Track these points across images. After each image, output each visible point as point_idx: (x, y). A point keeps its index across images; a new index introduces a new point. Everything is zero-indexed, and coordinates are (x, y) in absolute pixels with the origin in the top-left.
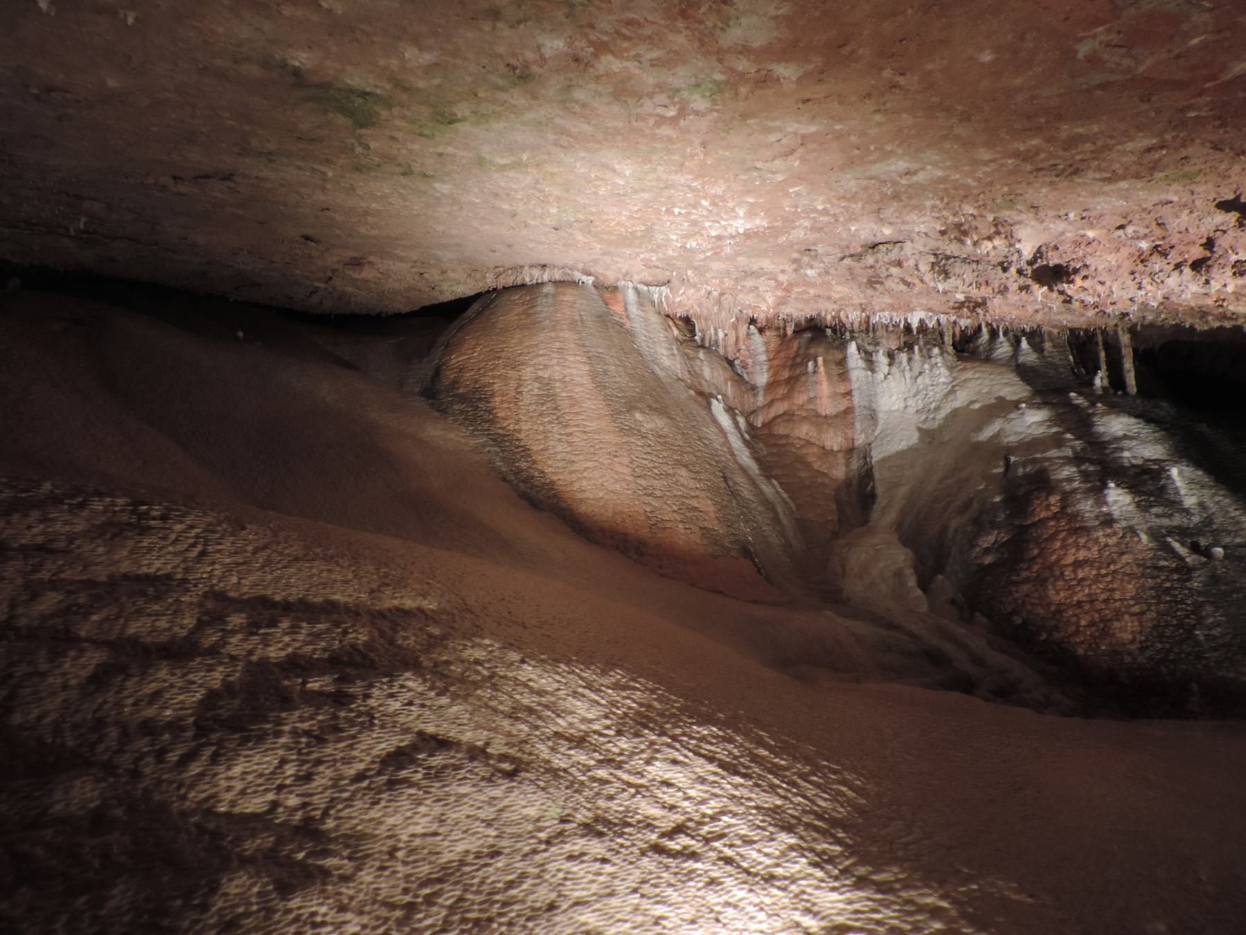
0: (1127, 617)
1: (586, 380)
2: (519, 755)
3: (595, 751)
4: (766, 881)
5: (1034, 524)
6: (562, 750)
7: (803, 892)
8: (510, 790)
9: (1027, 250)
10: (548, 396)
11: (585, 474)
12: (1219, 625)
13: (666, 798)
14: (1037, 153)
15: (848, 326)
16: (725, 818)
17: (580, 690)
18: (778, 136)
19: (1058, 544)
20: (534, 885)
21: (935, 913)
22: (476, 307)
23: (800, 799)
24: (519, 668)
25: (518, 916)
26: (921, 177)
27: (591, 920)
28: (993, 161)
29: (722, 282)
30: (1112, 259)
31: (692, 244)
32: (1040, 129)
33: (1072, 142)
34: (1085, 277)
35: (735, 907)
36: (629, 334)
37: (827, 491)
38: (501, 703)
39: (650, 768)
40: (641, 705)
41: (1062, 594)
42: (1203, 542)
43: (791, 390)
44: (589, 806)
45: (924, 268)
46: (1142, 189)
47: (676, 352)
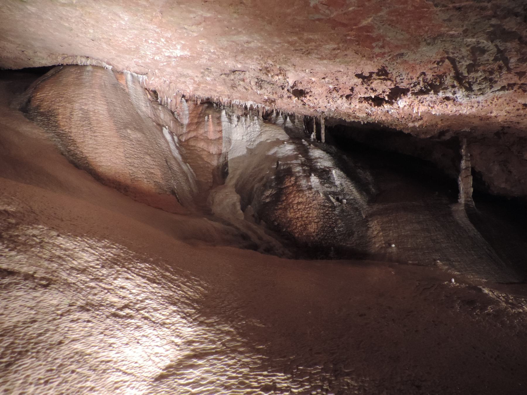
0: (313, 223)
1: (105, 113)
2: (51, 277)
3: (90, 275)
4: (161, 325)
5: (285, 188)
6: (74, 275)
7: (177, 329)
8: (44, 293)
9: (291, 82)
10: (86, 117)
11: (102, 155)
12: (342, 227)
13: (121, 294)
14: (296, 43)
15: (223, 103)
16: (147, 301)
17: (86, 248)
18: (194, 15)
19: (292, 196)
20: (53, 334)
21: (228, 333)
22: (52, 71)
23: (181, 292)
24: (56, 239)
25: (43, 348)
26: (252, 45)
27: (79, 347)
28: (280, 43)
29: (170, 77)
30: (320, 90)
31: (157, 58)
32: (296, 33)
33: (308, 41)
34: (310, 96)
35: (147, 337)
36: (128, 95)
37: (209, 170)
38: (44, 254)
39: (115, 281)
40: (115, 255)
41: (292, 214)
42: (340, 197)
43: (197, 127)
44: (84, 298)
45: (253, 83)
46: (332, 64)
47: (148, 105)
